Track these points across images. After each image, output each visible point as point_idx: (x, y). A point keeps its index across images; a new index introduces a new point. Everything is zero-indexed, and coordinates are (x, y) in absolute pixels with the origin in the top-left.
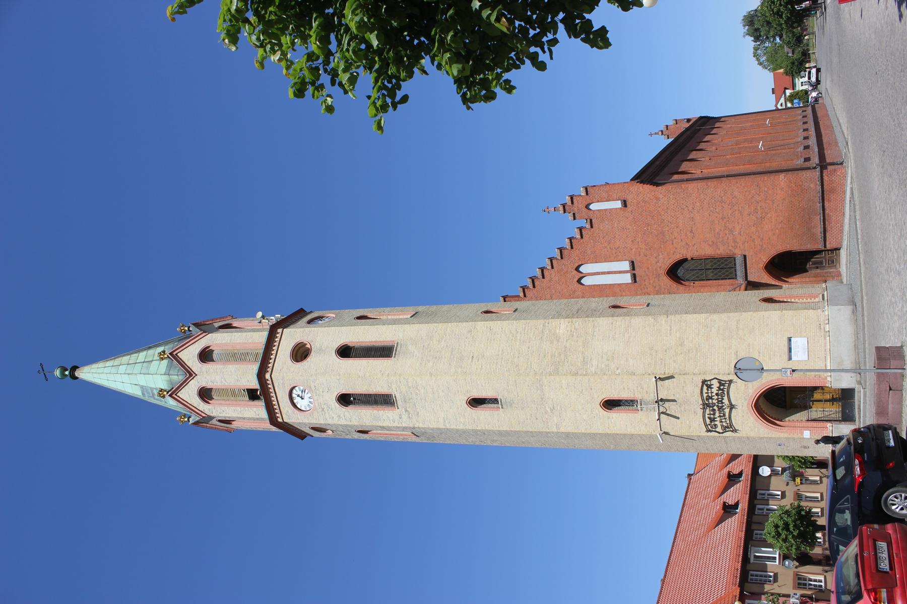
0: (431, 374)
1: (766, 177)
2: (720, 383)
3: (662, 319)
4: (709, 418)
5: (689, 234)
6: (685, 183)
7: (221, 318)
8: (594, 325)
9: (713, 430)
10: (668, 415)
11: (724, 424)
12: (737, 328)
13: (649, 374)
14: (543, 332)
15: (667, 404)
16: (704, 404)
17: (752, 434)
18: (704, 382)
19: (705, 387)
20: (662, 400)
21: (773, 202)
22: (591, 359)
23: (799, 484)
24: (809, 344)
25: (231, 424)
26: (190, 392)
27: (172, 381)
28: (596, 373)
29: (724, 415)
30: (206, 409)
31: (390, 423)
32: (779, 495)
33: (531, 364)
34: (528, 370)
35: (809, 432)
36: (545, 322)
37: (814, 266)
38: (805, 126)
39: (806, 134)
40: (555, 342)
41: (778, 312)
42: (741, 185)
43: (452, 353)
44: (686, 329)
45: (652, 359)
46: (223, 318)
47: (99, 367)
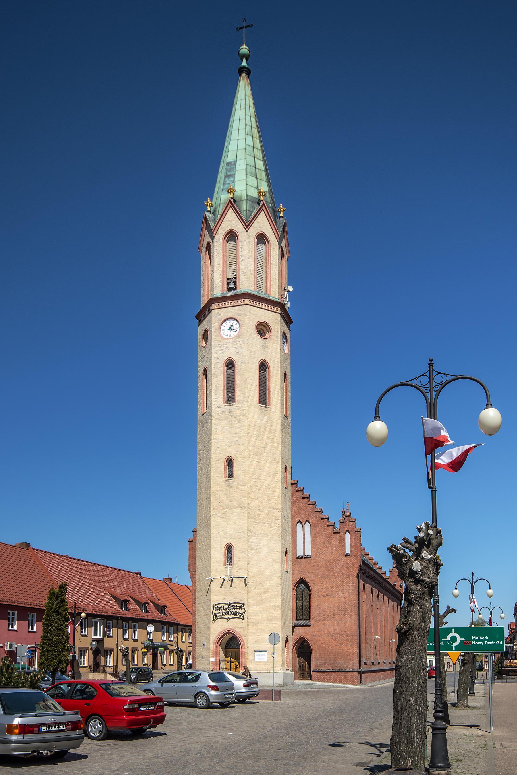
0: (248, 433)
1: (357, 641)
2: (243, 613)
3: (279, 581)
4: (221, 607)
5: (325, 594)
6: (358, 593)
7: (288, 247)
8: (277, 541)
9: (214, 608)
10: (223, 583)
11: (218, 615)
12: (273, 624)
13: (248, 574)
14: (273, 508)
15: (230, 582)
16: (230, 604)
17: (212, 630)
18: (243, 605)
19: (240, 605)
20: (232, 580)
21: (342, 644)
22: (257, 539)
23: (143, 651)
24: (263, 662)
25: (206, 251)
26: (233, 222)
27: (241, 202)
28: (249, 541)
29: (223, 615)
30: (220, 235)
31: (214, 399)
32: (32, 629)
33: (255, 501)
34: (251, 499)
35: (214, 660)
36: (279, 510)
37: (301, 665)
38: (387, 663)
39: (382, 663)
40: (267, 516)
41: (281, 646)
42: (353, 626)
43: (262, 447)
44: (273, 595)
45: (256, 575)
46: (289, 249)
47: (252, 118)
